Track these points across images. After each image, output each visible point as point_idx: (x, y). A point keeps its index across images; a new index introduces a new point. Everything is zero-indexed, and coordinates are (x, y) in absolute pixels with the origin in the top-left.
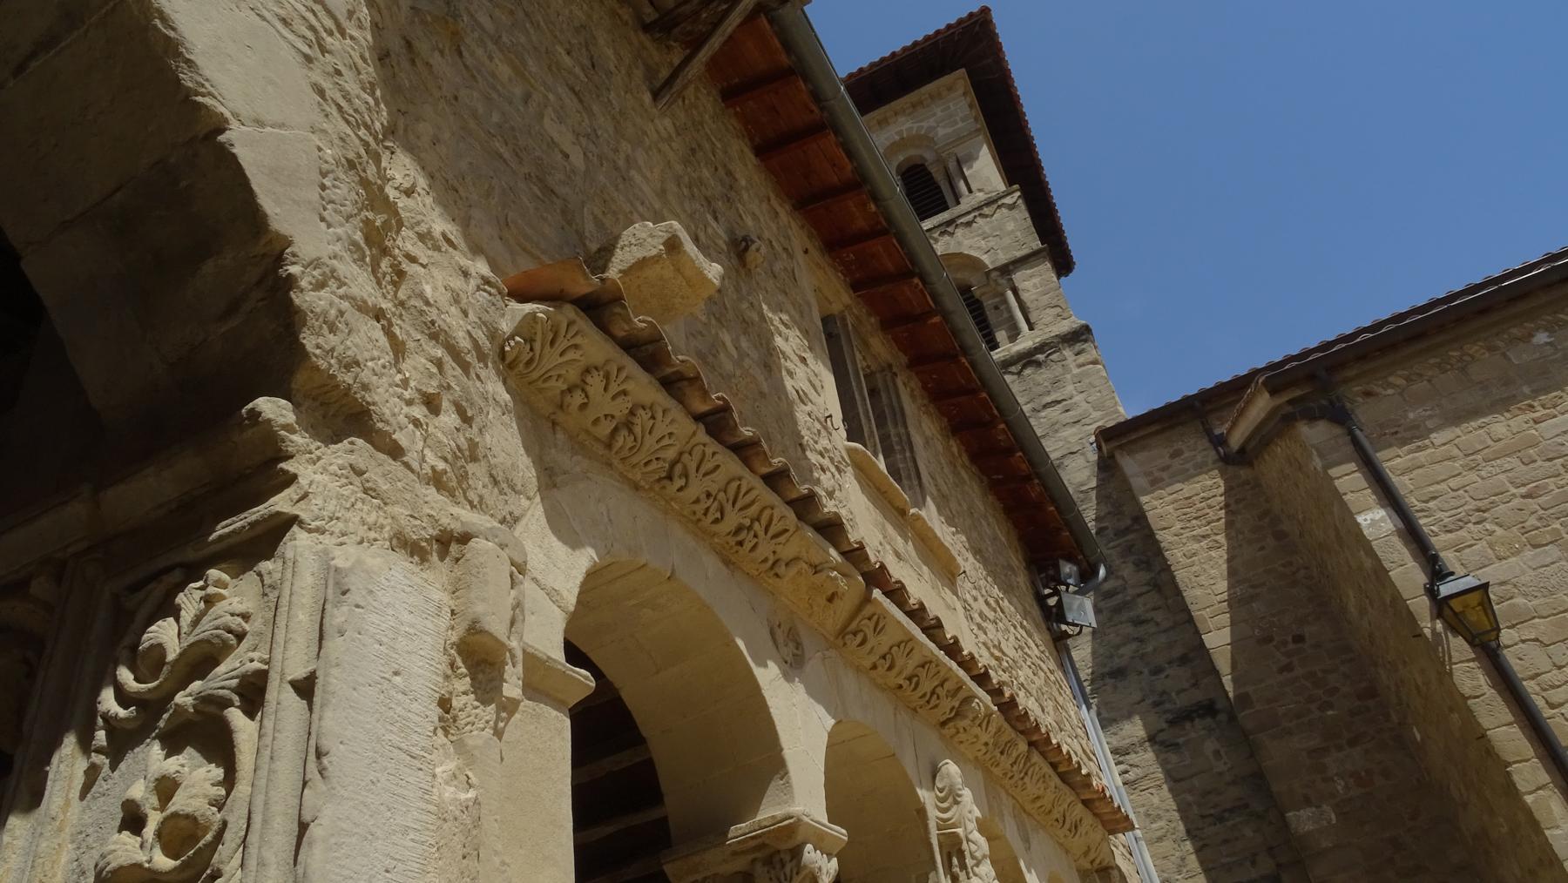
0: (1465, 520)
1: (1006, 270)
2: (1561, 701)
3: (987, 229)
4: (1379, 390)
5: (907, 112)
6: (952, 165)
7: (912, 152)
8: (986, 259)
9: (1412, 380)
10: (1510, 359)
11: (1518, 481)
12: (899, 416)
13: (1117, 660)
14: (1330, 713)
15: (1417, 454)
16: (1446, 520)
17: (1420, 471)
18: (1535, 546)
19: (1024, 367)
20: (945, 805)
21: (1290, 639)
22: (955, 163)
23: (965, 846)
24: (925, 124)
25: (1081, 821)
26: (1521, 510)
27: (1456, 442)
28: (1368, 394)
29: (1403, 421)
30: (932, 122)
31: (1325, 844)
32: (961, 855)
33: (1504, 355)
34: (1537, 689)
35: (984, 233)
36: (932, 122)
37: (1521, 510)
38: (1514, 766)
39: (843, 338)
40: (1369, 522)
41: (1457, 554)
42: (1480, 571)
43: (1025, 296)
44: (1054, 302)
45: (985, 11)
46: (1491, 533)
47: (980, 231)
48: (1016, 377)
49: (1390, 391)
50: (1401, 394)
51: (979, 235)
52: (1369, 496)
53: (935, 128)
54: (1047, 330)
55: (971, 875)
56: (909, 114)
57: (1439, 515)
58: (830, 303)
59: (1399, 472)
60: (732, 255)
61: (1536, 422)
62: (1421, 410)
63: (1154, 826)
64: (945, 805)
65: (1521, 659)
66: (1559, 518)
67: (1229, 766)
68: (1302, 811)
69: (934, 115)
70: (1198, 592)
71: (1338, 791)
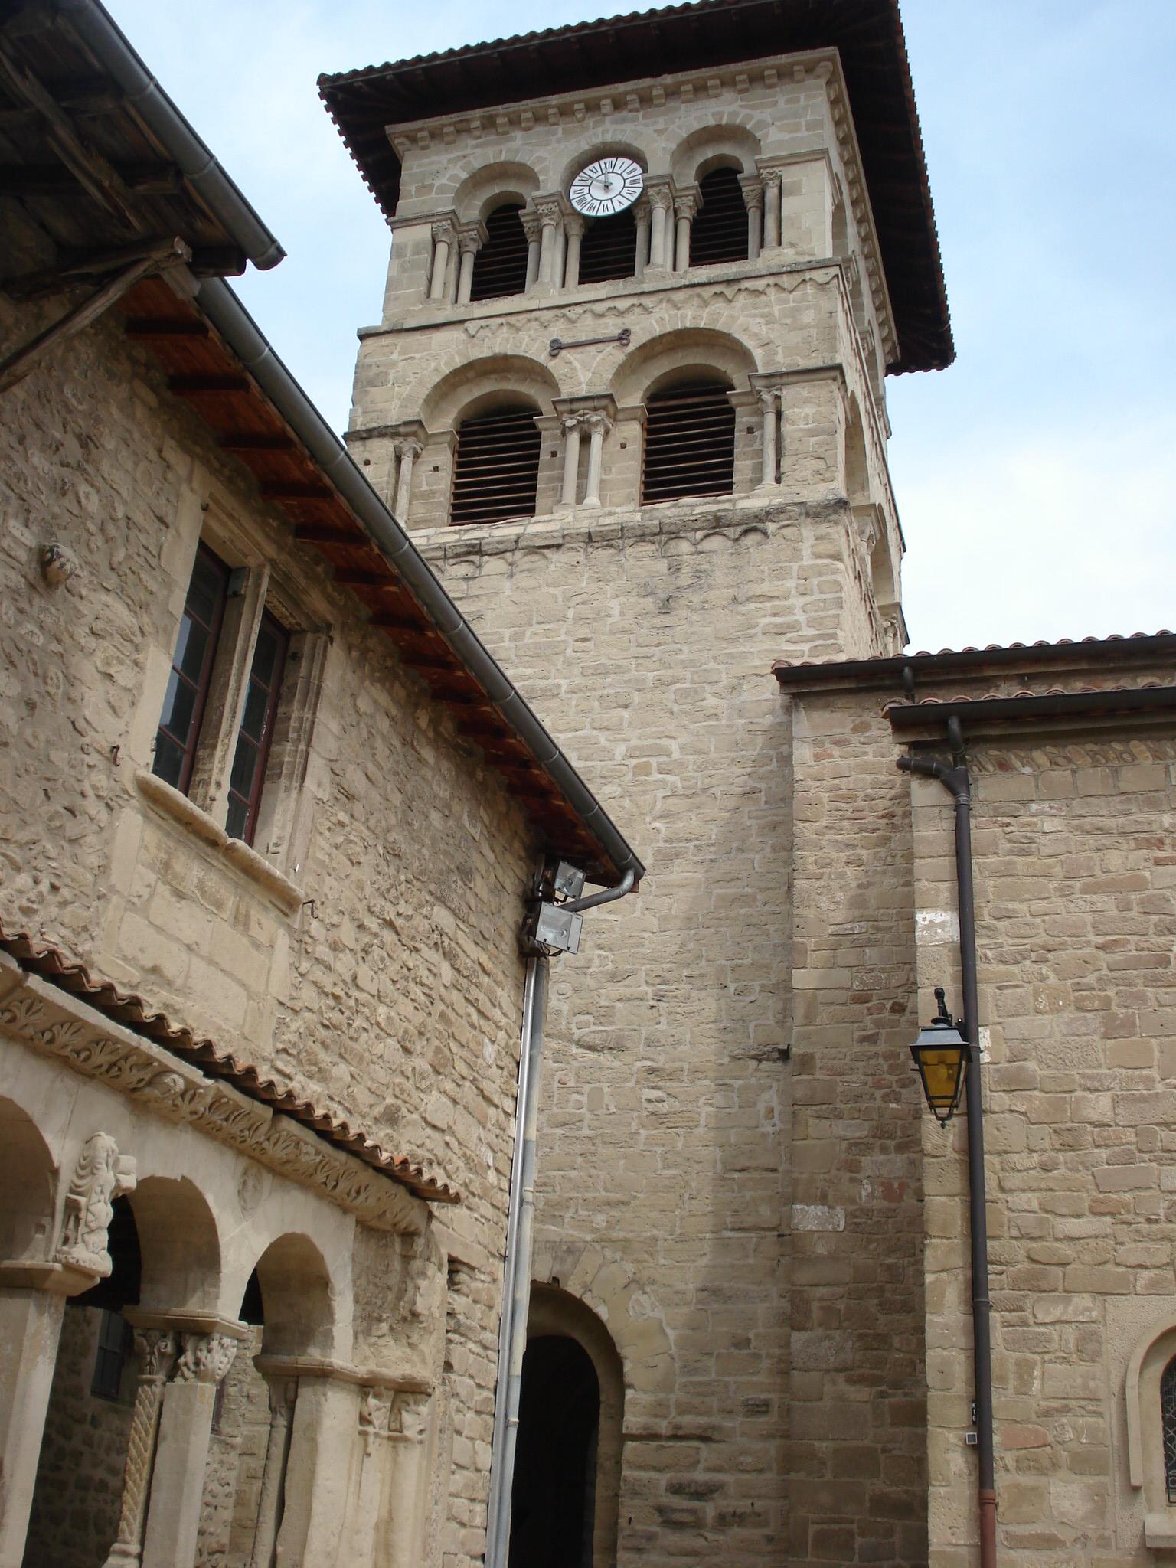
0: (1025, 954)
1: (776, 379)
2: (1014, 1188)
3: (776, 310)
4: (1018, 764)
5: (739, 87)
8: (758, 355)
9: (1057, 764)
11: (1101, 927)
12: (311, 696)
14: (893, 1105)
15: (1015, 858)
16: (1007, 948)
17: (1009, 879)
18: (1079, 1009)
19: (746, 532)
20: (82, 1173)
21: (889, 1005)
23: (82, 1214)
25: (366, 1187)
26: (1086, 962)
27: (1063, 858)
28: (1003, 766)
30: (766, 115)
31: (821, 1250)
32: (77, 1220)
34: (998, 1167)
35: (770, 314)
37: (1086, 962)
38: (933, 1240)
39: (248, 601)
40: (927, 923)
41: (998, 991)
42: (1010, 1019)
43: (786, 428)
44: (821, 451)
46: (1043, 978)
47: (766, 310)
48: (730, 543)
49: (1027, 770)
50: (1036, 778)
51: (762, 316)
52: (946, 890)
54: (796, 489)
55: (79, 1240)
56: (741, 92)
57: (1003, 939)
58: (246, 556)
59: (987, 874)
60: (168, 454)
61: (1158, 862)
63: (665, 1172)
64: (82, 1173)
65: (998, 1129)
66: (1118, 985)
67: (777, 1128)
68: (812, 1207)
69: (775, 104)
70: (811, 914)
71: (860, 1197)
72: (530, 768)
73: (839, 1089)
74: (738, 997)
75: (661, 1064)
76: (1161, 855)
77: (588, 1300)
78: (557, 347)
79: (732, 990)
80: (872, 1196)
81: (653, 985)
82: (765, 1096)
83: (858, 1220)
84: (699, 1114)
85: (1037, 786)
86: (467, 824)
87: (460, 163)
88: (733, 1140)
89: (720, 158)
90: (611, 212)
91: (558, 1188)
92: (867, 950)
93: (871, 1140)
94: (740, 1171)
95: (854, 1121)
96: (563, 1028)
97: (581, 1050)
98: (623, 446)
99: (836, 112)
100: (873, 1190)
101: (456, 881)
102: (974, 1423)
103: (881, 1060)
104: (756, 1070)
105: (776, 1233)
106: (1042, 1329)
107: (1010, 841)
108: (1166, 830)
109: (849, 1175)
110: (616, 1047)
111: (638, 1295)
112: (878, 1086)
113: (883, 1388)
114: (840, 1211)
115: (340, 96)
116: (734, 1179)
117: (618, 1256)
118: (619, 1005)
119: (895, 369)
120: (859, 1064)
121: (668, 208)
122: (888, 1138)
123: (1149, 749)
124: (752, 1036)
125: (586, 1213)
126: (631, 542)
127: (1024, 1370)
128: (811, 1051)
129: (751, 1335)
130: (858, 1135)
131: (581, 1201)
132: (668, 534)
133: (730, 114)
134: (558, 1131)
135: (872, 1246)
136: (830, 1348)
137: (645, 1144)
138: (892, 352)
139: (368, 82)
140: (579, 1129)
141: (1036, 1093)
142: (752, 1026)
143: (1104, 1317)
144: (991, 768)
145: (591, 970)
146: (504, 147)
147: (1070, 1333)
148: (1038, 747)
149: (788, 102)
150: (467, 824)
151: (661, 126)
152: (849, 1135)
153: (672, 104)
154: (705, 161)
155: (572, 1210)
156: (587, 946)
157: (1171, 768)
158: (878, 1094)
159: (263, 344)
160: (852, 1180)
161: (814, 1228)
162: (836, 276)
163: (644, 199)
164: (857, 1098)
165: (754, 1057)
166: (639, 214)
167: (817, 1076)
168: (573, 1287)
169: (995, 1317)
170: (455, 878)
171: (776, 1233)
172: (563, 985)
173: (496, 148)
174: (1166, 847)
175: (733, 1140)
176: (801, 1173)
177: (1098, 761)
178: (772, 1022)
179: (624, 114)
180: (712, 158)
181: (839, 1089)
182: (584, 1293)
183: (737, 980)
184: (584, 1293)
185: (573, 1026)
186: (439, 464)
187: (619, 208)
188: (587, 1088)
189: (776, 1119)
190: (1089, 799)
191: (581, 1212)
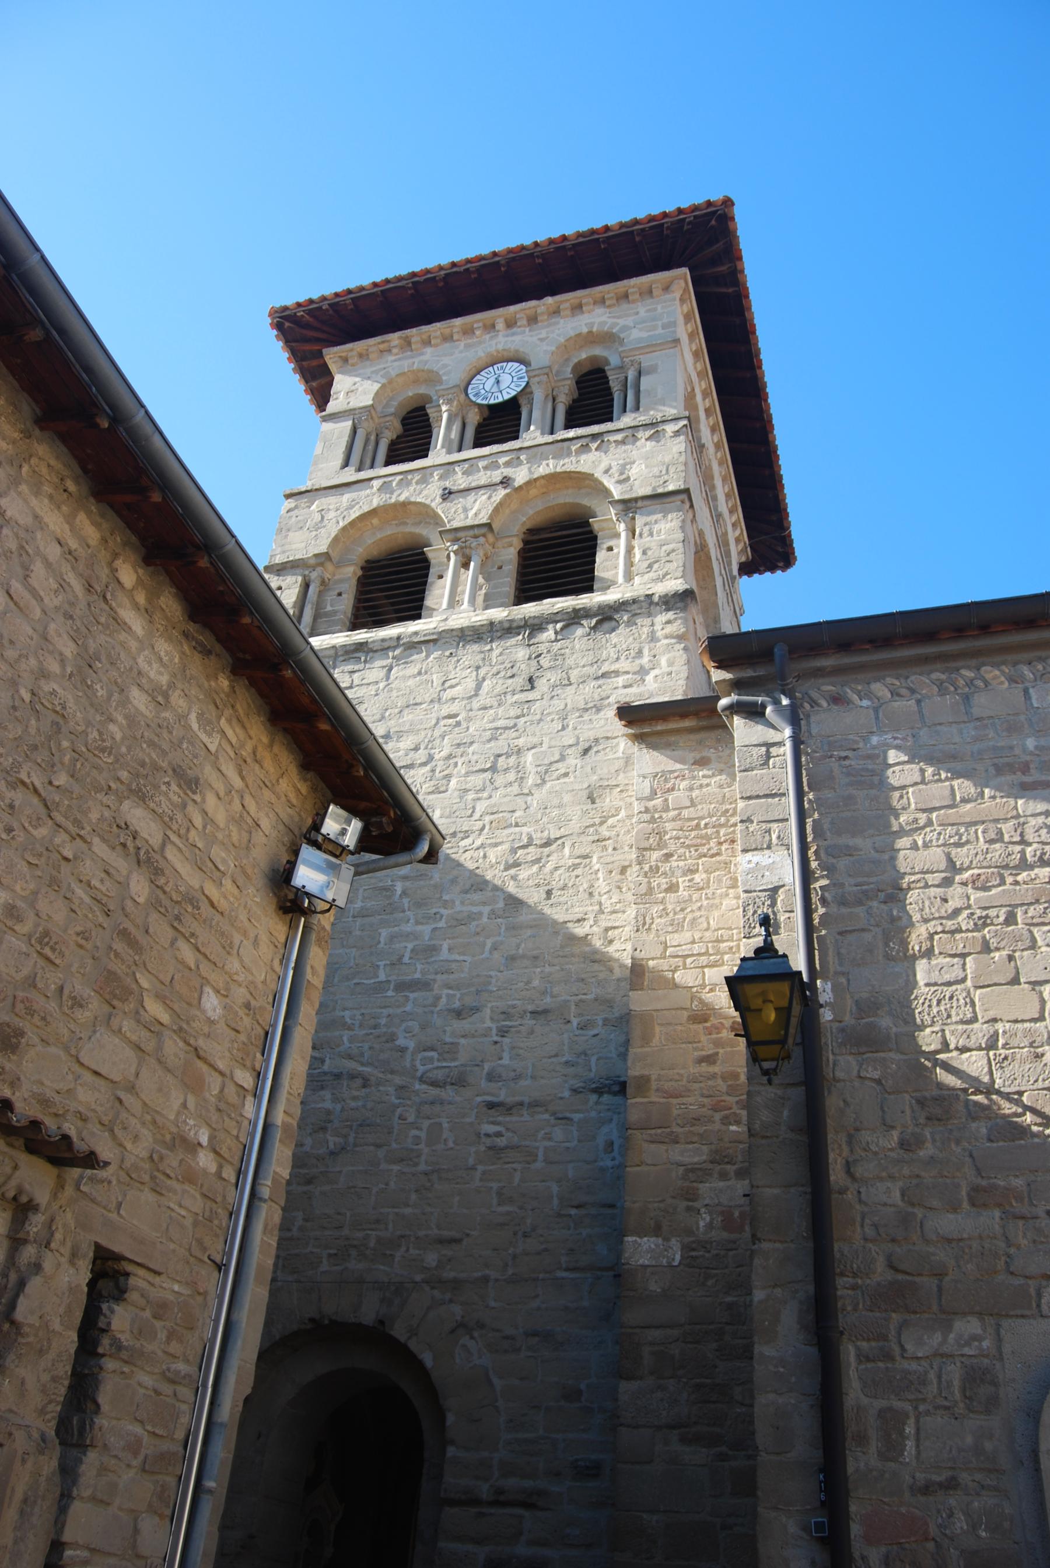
6: (631, 375)
7: (598, 351)
9: (899, 695)
10: (1030, 698)
13: (548, 1000)
14: (733, 1128)
22: (636, 374)
24: (621, 322)
28: (837, 700)
29: (861, 745)
30: (629, 321)
31: (654, 1287)
33: (1026, 691)
36: (629, 321)
40: (752, 865)
45: (728, 202)
49: (865, 703)
50: (876, 710)
53: (631, 328)
56: (609, 306)
62: (889, 736)
67: (617, 1162)
68: (645, 1239)
69: (637, 313)
71: (698, 1228)
72: (280, 670)
73: (675, 1112)
74: (581, 1032)
75: (501, 1098)
76: (1027, 779)
77: (413, 1345)
78: (448, 495)
79: (575, 1024)
80: (710, 1226)
81: (498, 1021)
82: (605, 1129)
83: (694, 1254)
84: (537, 1148)
85: (877, 718)
86: (195, 726)
87: (382, 373)
88: (571, 1174)
89: (593, 359)
90: (500, 400)
91: (391, 1226)
92: (706, 970)
93: (710, 1166)
94: (577, 1207)
95: (691, 1146)
96: (408, 1065)
97: (424, 1087)
98: (500, 568)
99: (689, 325)
100: (712, 1220)
101: (168, 784)
102: (823, 1503)
103: (720, 1081)
104: (597, 1103)
105: (611, 1273)
106: (914, 1366)
107: (848, 774)
108: (1031, 753)
109: (685, 1203)
110: (460, 1082)
111: (465, 1340)
112: (715, 1109)
113: (724, 1449)
114: (675, 1243)
115: (287, 324)
116: (570, 1216)
117: (448, 1296)
118: (462, 1041)
119: (747, 569)
120: (696, 1086)
121: (547, 396)
122: (728, 1163)
123: (1003, 672)
124: (594, 1070)
125: (417, 1252)
126: (499, 634)
127: (891, 1421)
128: (647, 1073)
129: (583, 1387)
130: (696, 1159)
131: (413, 1239)
132: (535, 626)
133: (600, 323)
134: (396, 1168)
135: (710, 1283)
136: (662, 1400)
137: (481, 1180)
138: (743, 551)
139: (310, 312)
140: (416, 1165)
141: (892, 1055)
142: (594, 1059)
143: (999, 1349)
144: (824, 704)
145: (438, 1008)
146: (416, 360)
147: (954, 1373)
148: (877, 680)
149: (648, 311)
150: (195, 726)
151: (543, 335)
152: (686, 1160)
153: (553, 320)
154: (579, 362)
155: (403, 1249)
156: (436, 986)
157: (1031, 690)
158: (718, 1116)
159: (229, 537)
160: (689, 1209)
161: (647, 1262)
162: (685, 426)
163: (528, 390)
164: (697, 1120)
165: (595, 1091)
166: (523, 402)
167: (654, 1099)
168: (399, 1332)
169: (849, 1352)
170: (167, 779)
171: (611, 1273)
172: (410, 1023)
173: (410, 361)
174: (1032, 771)
175: (571, 1174)
176: (634, 1202)
177: (947, 688)
178: (614, 1056)
179: (515, 330)
180: (586, 359)
181: (675, 1112)
182: (409, 1338)
183: (580, 1015)
184: (409, 1338)
185: (418, 1063)
186: (342, 590)
187: (507, 397)
188: (426, 1124)
189: (615, 1153)
190: (939, 728)
191: (412, 1251)
